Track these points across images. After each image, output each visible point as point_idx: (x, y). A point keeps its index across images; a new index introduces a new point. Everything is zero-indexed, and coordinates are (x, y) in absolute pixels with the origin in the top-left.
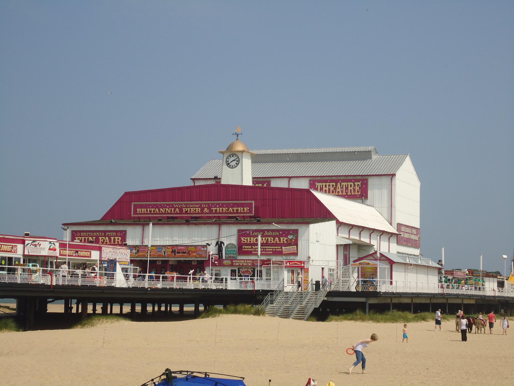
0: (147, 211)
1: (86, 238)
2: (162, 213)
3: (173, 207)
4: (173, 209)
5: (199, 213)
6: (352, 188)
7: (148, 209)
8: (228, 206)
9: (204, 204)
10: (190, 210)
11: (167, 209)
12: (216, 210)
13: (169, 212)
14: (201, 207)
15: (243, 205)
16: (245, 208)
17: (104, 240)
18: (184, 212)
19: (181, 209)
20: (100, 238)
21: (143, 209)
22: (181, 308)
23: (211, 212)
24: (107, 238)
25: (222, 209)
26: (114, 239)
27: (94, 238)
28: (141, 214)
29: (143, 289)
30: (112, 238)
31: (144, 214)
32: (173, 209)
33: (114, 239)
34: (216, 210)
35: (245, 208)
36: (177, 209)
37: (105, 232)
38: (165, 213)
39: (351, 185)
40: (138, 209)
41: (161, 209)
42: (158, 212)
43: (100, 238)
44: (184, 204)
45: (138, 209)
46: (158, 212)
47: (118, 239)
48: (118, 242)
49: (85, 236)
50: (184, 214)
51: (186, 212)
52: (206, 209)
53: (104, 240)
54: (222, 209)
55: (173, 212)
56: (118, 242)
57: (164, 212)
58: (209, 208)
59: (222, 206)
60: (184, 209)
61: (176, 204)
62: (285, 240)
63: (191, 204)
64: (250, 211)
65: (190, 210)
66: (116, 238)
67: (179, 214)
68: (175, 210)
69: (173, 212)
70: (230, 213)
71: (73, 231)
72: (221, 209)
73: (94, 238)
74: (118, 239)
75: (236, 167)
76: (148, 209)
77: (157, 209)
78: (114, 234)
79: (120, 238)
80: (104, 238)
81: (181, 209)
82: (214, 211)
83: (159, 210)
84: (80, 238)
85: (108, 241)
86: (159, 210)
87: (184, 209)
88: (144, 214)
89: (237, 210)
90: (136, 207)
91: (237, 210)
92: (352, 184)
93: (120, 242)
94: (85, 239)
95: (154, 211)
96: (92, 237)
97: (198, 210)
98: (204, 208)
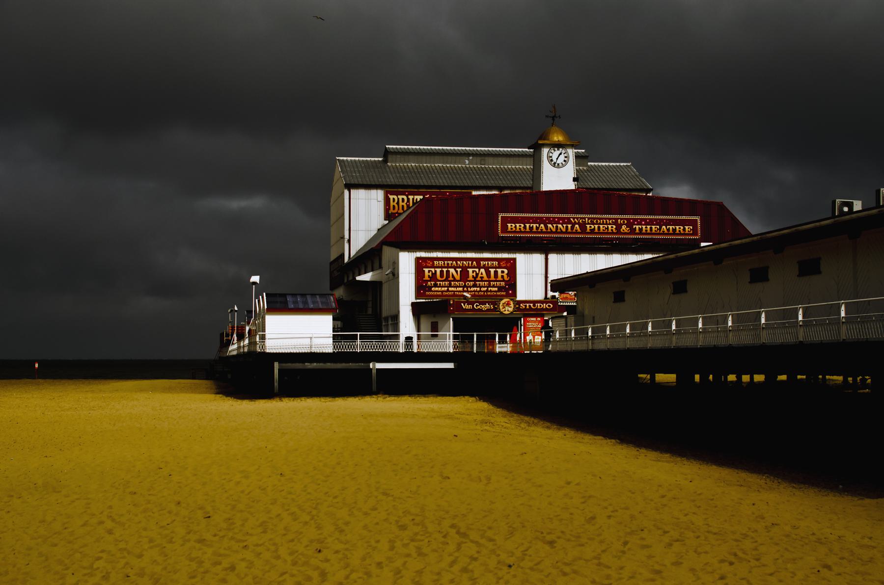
0: (525, 227)
1: (445, 270)
2: (552, 232)
3: (570, 222)
4: (569, 226)
5: (613, 233)
6: (404, 204)
7: (528, 225)
8: (660, 223)
9: (621, 219)
10: (599, 228)
11: (560, 226)
12: (641, 230)
13: (564, 230)
14: (616, 223)
15: (683, 223)
16: (687, 227)
17: (477, 274)
18: (588, 230)
19: (583, 226)
20: (470, 270)
21: (518, 225)
22: (752, 378)
23: (633, 231)
24: (483, 270)
25: (651, 228)
26: (496, 272)
27: (459, 270)
28: (515, 232)
29: (506, 353)
30: (492, 271)
31: (520, 232)
32: (569, 226)
33: (496, 272)
34: (641, 230)
35: (687, 227)
36: (577, 226)
37: (478, 260)
38: (556, 232)
39: (403, 200)
40: (509, 225)
41: (550, 226)
42: (544, 230)
43: (470, 270)
44: (589, 219)
45: (509, 225)
46: (544, 230)
47: (503, 272)
48: (502, 277)
49: (442, 267)
50: (588, 233)
51: (592, 231)
52: (624, 227)
53: (477, 274)
54: (651, 228)
55: (569, 230)
56: (502, 277)
57: (554, 230)
58: (630, 224)
59: (651, 222)
60: (588, 226)
61: (574, 218)
62: (505, 275)
63: (600, 219)
64: (695, 232)
65: (599, 228)
66: (499, 270)
67: (579, 233)
68: (572, 228)
69: (569, 230)
70: (663, 234)
71: (418, 259)
72: (649, 227)
73: (459, 270)
74: (503, 272)
75: (563, 166)
76: (528, 225)
77: (542, 225)
78: (496, 263)
79: (506, 271)
80: (477, 270)
81: (583, 226)
82: (637, 231)
83: (546, 227)
84: (433, 270)
85: (484, 275)
86: (546, 227)
87: (588, 226)
88: (520, 232)
89: (674, 230)
90: (505, 221)
91: (674, 230)
92: (405, 197)
93: (505, 277)
94: (442, 272)
95: (537, 228)
96: (455, 268)
97: (612, 228)
98: (621, 225)
